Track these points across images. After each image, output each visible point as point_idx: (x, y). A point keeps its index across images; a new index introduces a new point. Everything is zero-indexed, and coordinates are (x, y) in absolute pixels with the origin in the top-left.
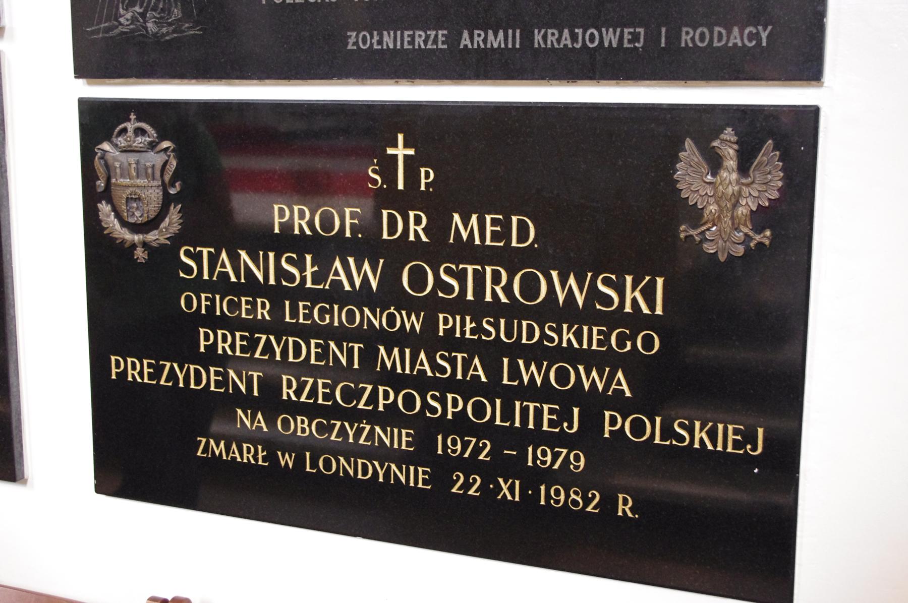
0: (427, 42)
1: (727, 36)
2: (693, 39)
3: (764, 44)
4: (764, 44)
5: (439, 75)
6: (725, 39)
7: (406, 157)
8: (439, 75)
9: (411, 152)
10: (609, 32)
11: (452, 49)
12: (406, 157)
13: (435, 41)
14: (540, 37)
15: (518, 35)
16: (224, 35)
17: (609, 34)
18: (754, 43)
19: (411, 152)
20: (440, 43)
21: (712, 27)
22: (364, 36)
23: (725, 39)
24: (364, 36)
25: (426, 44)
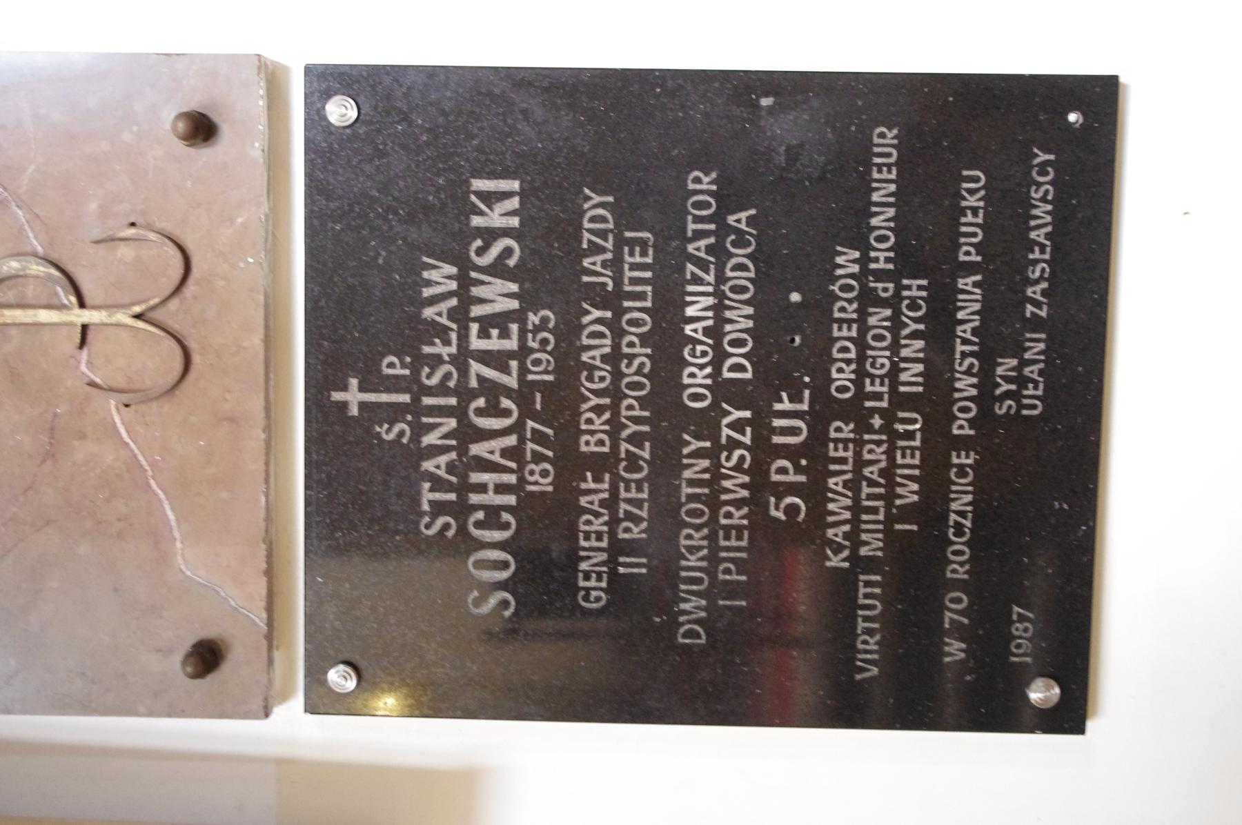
0: (592, 430)
1: (632, 311)
2: (962, 564)
3: (1052, 157)
4: (1052, 157)
5: (313, 328)
6: (953, 606)
7: (362, 389)
8: (313, 328)
9: (354, 382)
10: (483, 295)
11: (331, 285)
12: (362, 389)
13: (638, 503)
14: (972, 199)
15: (628, 560)
16: (674, 213)
17: (491, 296)
18: (1050, 169)
19: (354, 382)
20: (640, 496)
21: (542, 389)
22: (709, 205)
23: (953, 606)
24: (709, 205)
25: (641, 519)
